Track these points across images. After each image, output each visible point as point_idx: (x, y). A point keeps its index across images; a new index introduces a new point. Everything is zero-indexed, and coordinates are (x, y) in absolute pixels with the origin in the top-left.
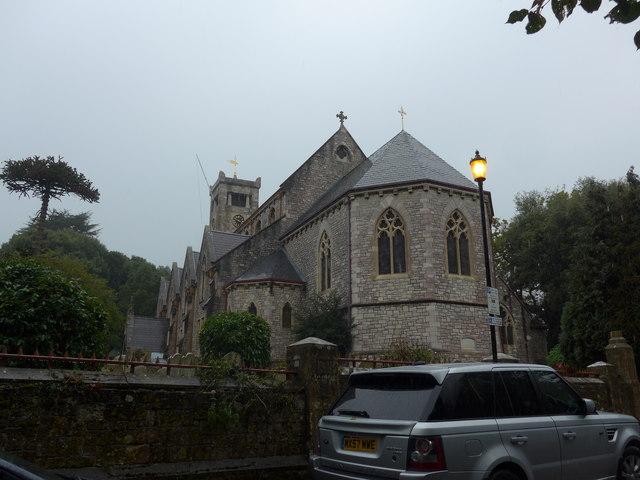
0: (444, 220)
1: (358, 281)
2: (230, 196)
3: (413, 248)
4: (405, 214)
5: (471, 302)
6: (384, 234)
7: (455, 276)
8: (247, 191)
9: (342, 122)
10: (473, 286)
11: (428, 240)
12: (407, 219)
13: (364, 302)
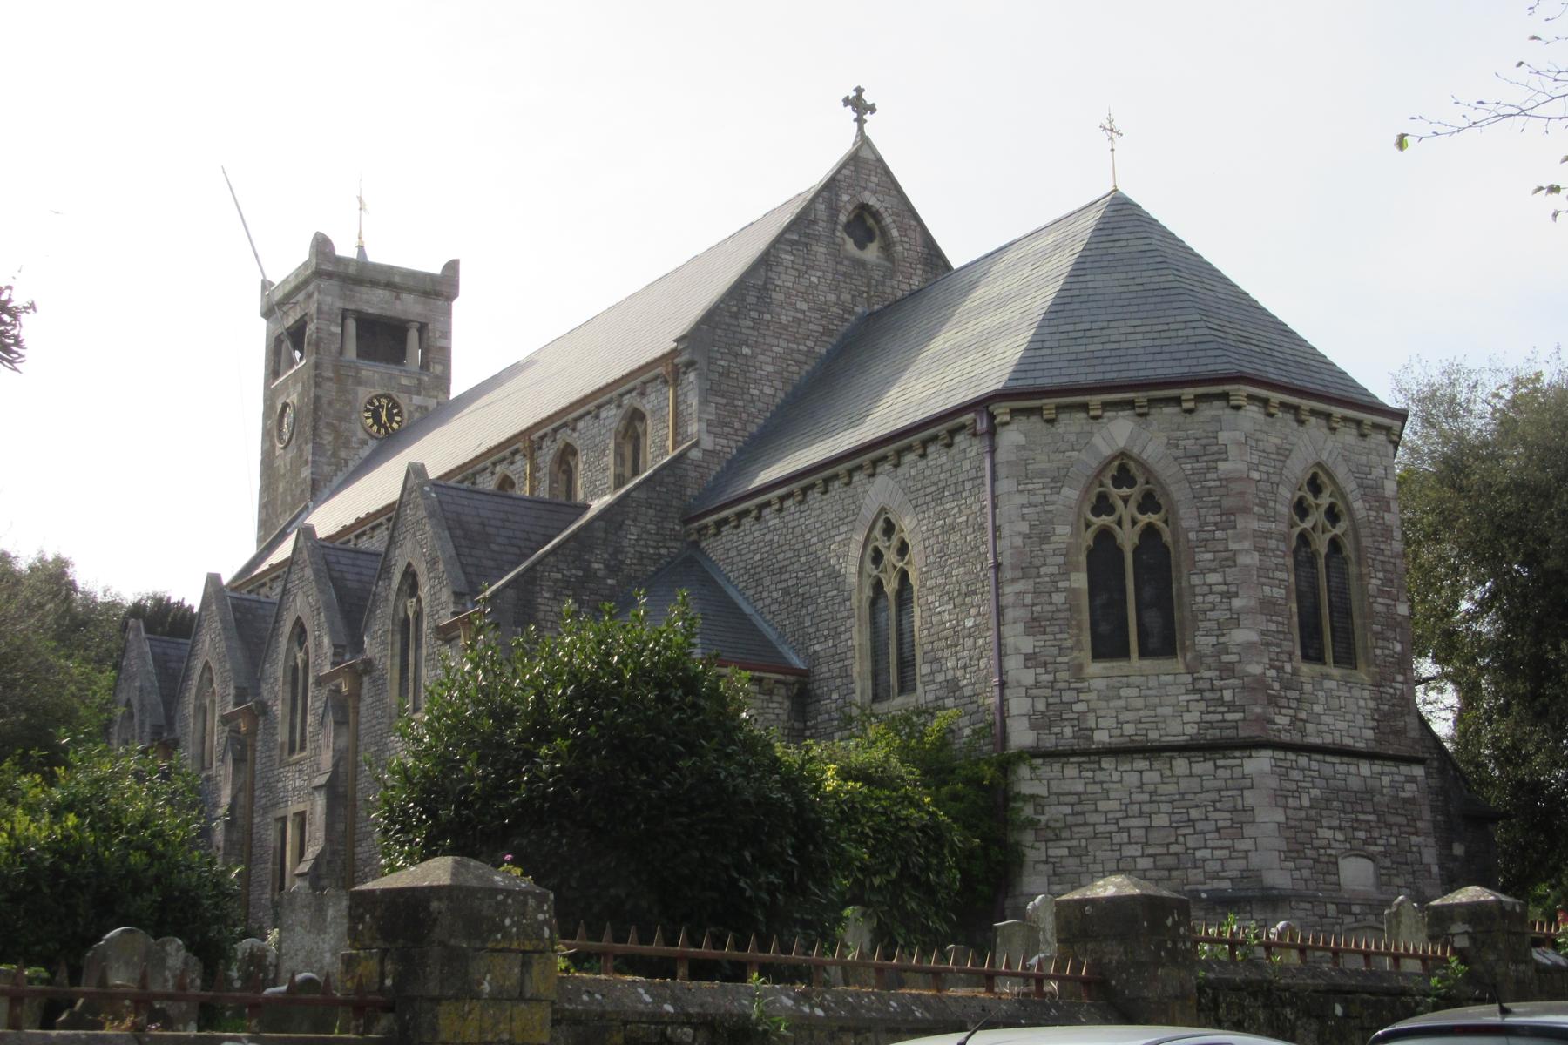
0: (1286, 494)
1: (1028, 677)
2: (352, 326)
4: (1169, 473)
5: (1361, 745)
6: (1105, 536)
7: (1318, 668)
8: (409, 307)
9: (860, 121)
11: (1243, 560)
12: (1179, 493)
13: (1049, 742)
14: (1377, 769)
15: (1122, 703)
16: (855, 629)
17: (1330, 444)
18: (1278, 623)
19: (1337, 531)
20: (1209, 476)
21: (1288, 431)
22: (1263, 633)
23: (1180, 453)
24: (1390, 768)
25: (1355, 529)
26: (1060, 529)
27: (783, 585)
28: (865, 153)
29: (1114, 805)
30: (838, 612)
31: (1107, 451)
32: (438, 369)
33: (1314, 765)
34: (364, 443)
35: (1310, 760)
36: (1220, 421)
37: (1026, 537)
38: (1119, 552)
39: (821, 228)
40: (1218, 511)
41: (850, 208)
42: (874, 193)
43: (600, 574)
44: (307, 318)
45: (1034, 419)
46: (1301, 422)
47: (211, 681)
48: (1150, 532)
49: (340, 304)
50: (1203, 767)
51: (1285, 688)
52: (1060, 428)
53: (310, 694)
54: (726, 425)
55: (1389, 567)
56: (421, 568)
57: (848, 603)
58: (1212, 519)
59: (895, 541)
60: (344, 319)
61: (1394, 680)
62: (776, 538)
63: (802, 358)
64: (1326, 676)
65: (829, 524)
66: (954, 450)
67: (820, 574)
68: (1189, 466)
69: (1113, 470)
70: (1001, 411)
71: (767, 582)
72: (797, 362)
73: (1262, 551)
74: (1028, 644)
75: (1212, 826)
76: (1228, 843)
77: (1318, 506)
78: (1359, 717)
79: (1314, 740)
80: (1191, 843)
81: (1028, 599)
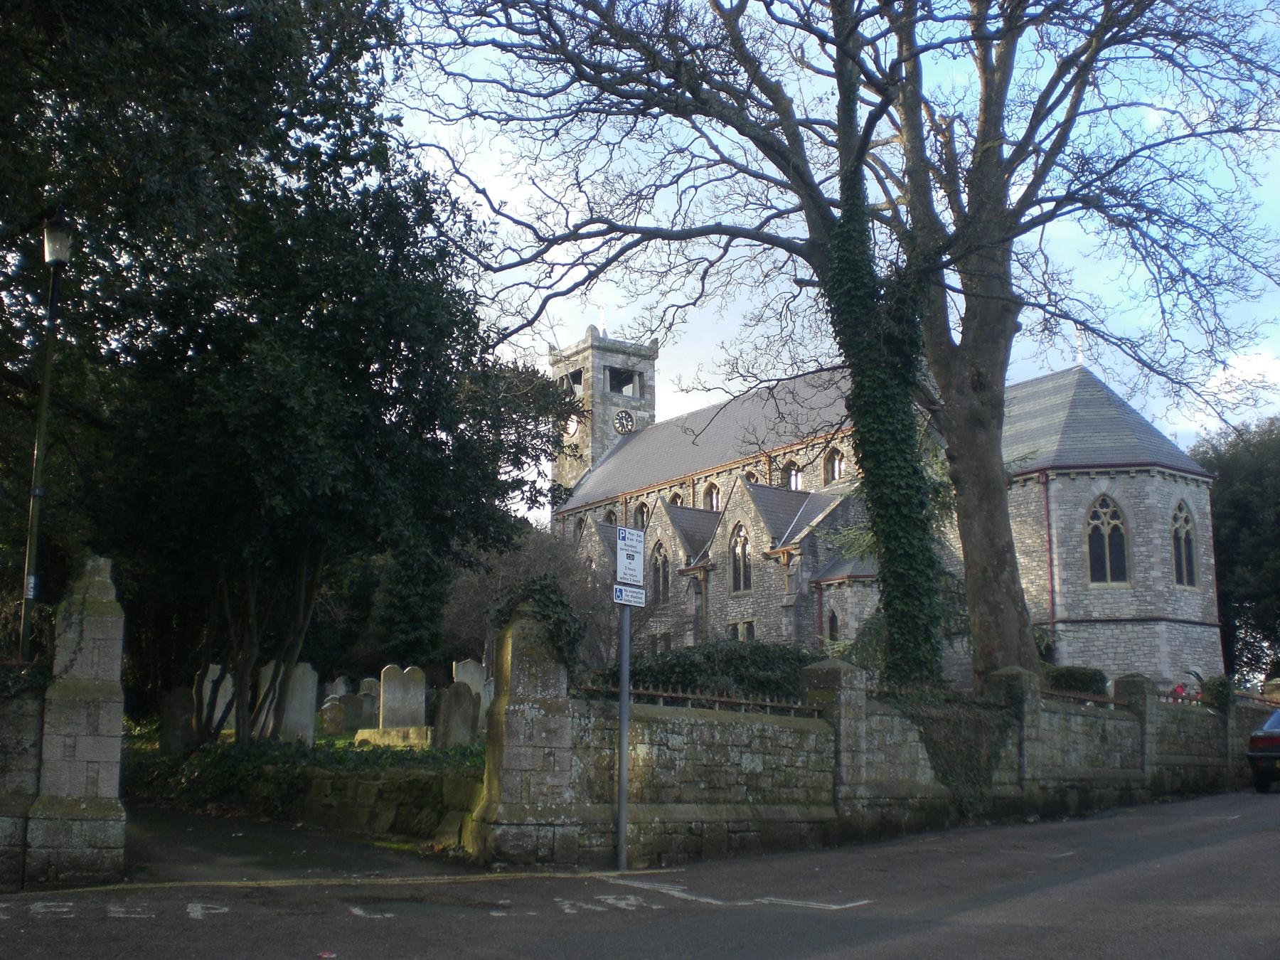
0: (1171, 513)
2: (608, 373)
3: (1136, 551)
4: (1123, 503)
5: (1197, 620)
10: (1197, 601)
12: (1128, 512)
13: (1073, 617)
22: (1163, 573)
24: (1207, 629)
25: (1194, 528)
26: (1077, 526)
29: (1101, 643)
31: (1097, 493)
32: (648, 396)
34: (616, 437)
37: (1063, 529)
38: (1102, 536)
45: (1066, 478)
46: (1176, 481)
48: (1115, 528)
50: (1138, 628)
52: (1077, 482)
66: (1026, 488)
69: (1099, 502)
70: (1052, 475)
73: (1162, 537)
79: (1181, 618)
80: (1133, 659)
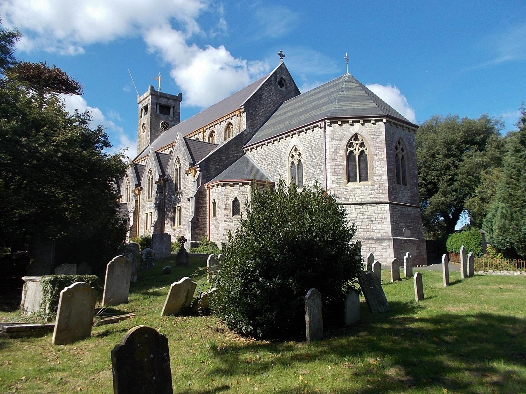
2: (158, 106)
8: (171, 103)
14: (411, 209)
15: (356, 192)
16: (287, 174)
17: (403, 133)
18: (392, 175)
19: (403, 154)
20: (377, 139)
21: (394, 129)
23: (370, 133)
27: (268, 163)
28: (283, 66)
29: (354, 216)
30: (282, 169)
33: (399, 208)
35: (398, 207)
36: (380, 126)
39: (273, 82)
40: (379, 147)
41: (279, 78)
42: (284, 75)
43: (224, 159)
44: (148, 105)
46: (397, 128)
47: (129, 183)
49: (156, 101)
51: (393, 190)
53: (153, 186)
54: (252, 126)
55: (414, 162)
56: (180, 157)
57: (285, 167)
58: (378, 149)
59: (297, 153)
60: (157, 105)
61: (414, 189)
62: (266, 152)
63: (269, 112)
64: (401, 187)
65: (280, 149)
67: (278, 160)
68: (373, 137)
71: (264, 162)
72: (268, 113)
74: (333, 178)
75: (377, 222)
76: (381, 226)
77: (400, 147)
78: (408, 197)
81: (334, 167)
